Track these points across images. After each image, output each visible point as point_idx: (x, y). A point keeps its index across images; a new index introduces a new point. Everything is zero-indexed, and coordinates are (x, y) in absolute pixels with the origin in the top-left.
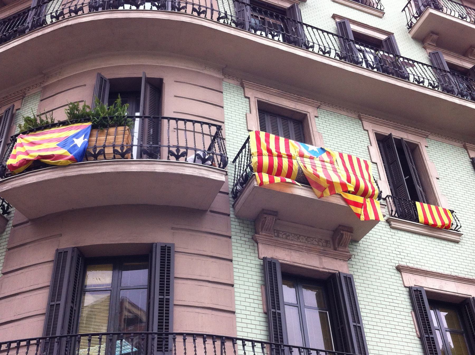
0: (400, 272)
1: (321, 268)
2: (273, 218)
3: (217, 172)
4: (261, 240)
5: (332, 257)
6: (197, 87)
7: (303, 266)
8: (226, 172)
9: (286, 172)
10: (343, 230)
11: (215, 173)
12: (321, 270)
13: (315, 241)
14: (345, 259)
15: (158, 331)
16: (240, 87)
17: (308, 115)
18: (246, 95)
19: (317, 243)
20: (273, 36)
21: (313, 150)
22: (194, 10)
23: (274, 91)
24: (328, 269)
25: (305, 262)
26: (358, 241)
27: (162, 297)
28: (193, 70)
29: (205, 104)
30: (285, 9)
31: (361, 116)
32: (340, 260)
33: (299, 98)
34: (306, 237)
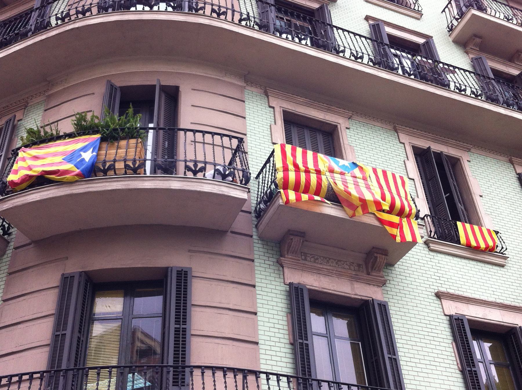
0: (440, 299)
1: (352, 294)
2: (300, 240)
3: (238, 189)
4: (286, 263)
5: (365, 282)
6: (216, 95)
7: (333, 292)
8: (249, 189)
9: (315, 188)
10: (377, 253)
11: (237, 191)
12: (353, 296)
14: (379, 285)
15: (174, 364)
16: (264, 96)
17: (339, 126)
18: (270, 105)
19: (348, 267)
20: (300, 40)
21: (344, 165)
22: (213, 11)
23: (301, 100)
24: (360, 296)
25: (335, 288)
26: (394, 265)
27: (178, 326)
28: (212, 76)
29: (225, 114)
30: (313, 10)
31: (397, 128)
32: (374, 285)
33: (329, 107)
34: (337, 261)
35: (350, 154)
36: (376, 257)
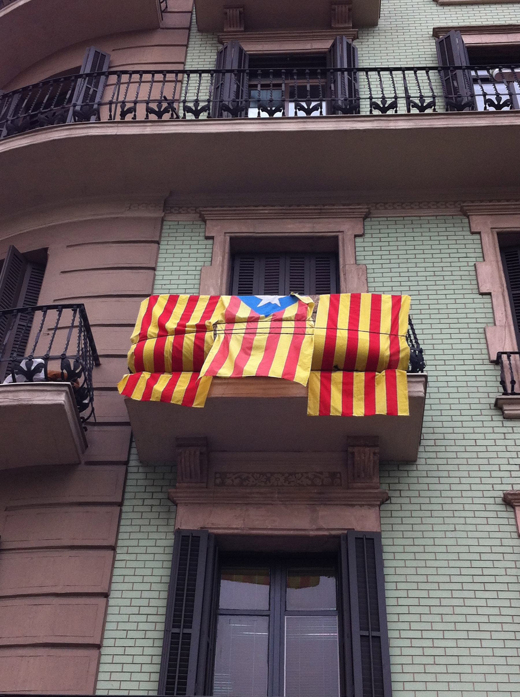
0: (513, 507)
1: (312, 530)
2: (195, 452)
3: (49, 391)
4: (181, 497)
5: (343, 503)
6: (107, 245)
7: (270, 532)
8: (426, 377)
9: (191, 358)
10: (353, 446)
11: (46, 393)
12: (312, 533)
13: (307, 478)
14: (372, 503)
15: (166, 694)
16: (199, 223)
17: (340, 238)
18: (472, 230)
19: (309, 482)
20: (308, 111)
21: (270, 303)
22: (150, 111)
23: (267, 212)
24: (328, 529)
25: (277, 525)
26: (415, 461)
27: (186, 631)
28: (105, 216)
29: (117, 271)
30: (325, 53)
31: (203, 213)
32: (361, 506)
33: (321, 209)
34: (287, 475)
35: (356, 280)
36: (353, 453)
